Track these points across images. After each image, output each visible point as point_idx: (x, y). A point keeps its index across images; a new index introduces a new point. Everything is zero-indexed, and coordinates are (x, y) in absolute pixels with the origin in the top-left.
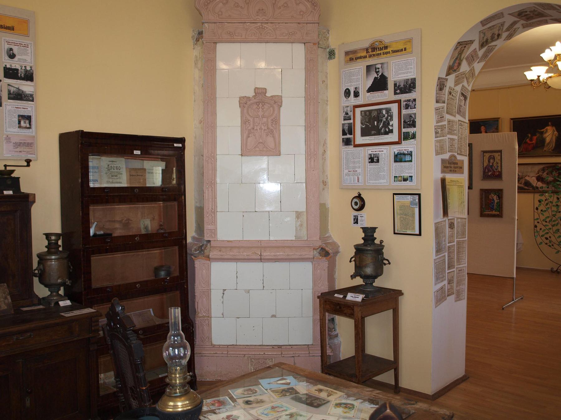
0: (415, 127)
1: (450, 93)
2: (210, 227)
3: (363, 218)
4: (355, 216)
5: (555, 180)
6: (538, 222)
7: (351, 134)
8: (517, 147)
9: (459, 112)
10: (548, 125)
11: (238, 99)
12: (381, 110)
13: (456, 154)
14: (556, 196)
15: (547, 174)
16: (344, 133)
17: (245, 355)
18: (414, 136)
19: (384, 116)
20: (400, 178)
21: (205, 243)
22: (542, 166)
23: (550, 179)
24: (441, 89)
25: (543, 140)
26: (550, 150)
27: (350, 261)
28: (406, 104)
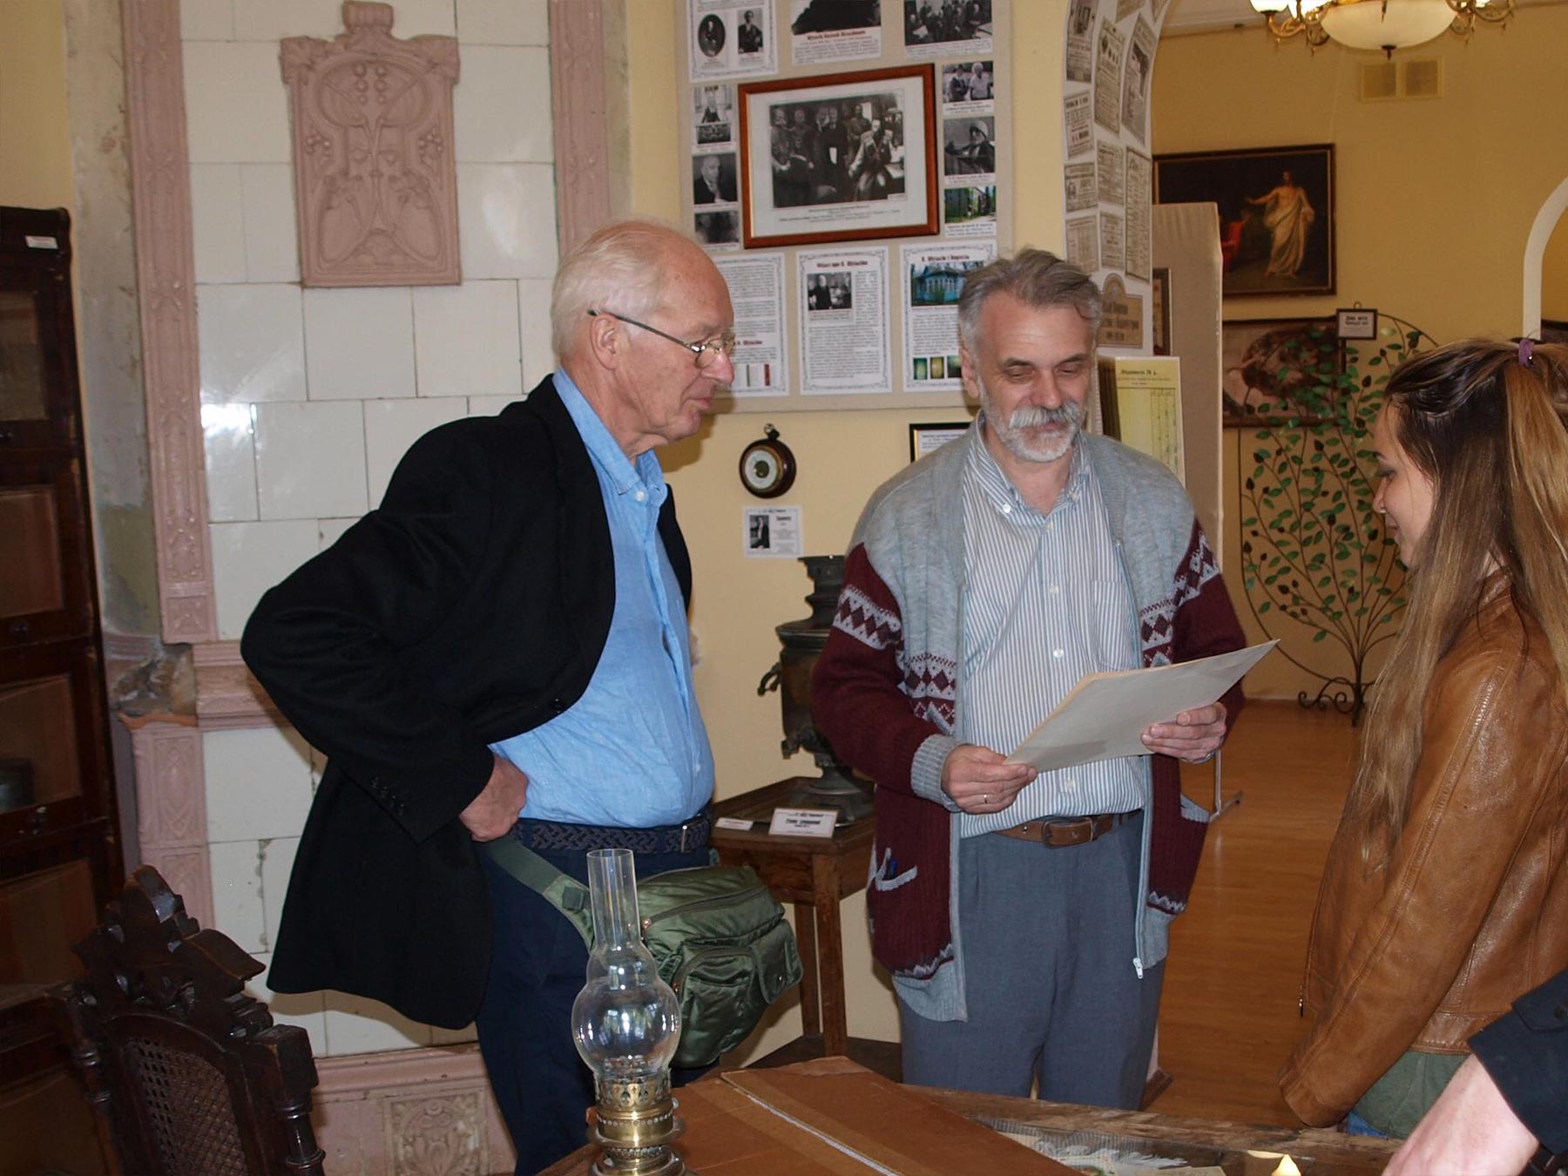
0: (990, 168)
1: (1105, 45)
2: (180, 588)
3: (789, 525)
4: (756, 518)
5: (1309, 382)
6: (1255, 533)
7: (730, 195)
8: (1219, 259)
9: (1128, 118)
10: (1281, 184)
11: (275, 50)
12: (855, 102)
13: (1121, 274)
14: (1312, 437)
15: (1282, 359)
16: (702, 194)
17: (366, 1091)
18: (987, 206)
19: (868, 127)
20: (937, 366)
21: (162, 655)
22: (1262, 332)
23: (1292, 376)
24: (1080, 28)
25: (1267, 236)
26: (1290, 273)
27: (762, 691)
28: (955, 83)
